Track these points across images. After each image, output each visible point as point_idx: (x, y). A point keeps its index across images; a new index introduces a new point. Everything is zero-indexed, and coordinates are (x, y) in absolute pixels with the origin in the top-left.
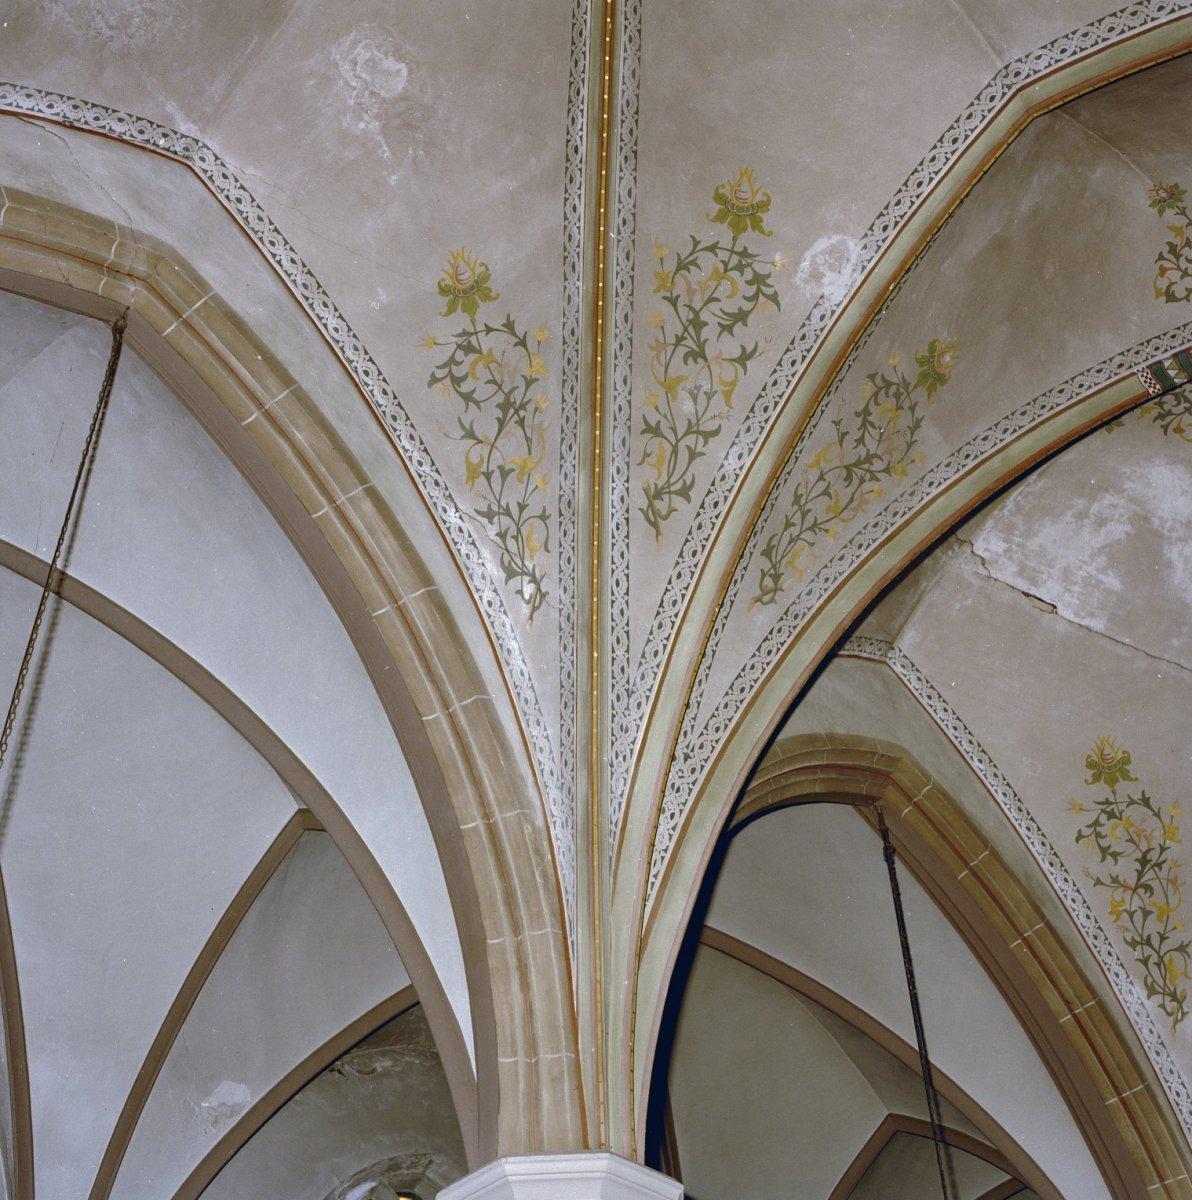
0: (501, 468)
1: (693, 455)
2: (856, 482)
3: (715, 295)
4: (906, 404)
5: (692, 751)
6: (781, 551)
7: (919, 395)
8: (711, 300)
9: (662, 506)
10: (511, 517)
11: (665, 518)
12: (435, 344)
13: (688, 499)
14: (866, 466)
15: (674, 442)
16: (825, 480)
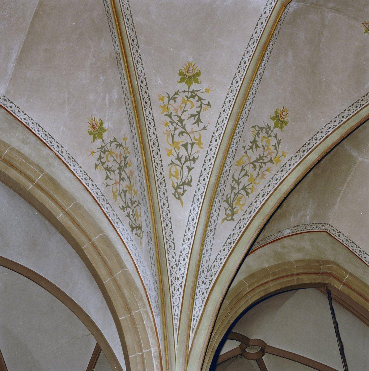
0: (123, 190)
1: (190, 169)
2: (258, 168)
3: (185, 109)
4: (273, 135)
5: (211, 268)
6: (232, 199)
7: (277, 130)
8: (184, 111)
9: (180, 191)
10: (129, 207)
11: (183, 194)
12: (94, 153)
13: (191, 186)
14: (261, 161)
15: (181, 166)
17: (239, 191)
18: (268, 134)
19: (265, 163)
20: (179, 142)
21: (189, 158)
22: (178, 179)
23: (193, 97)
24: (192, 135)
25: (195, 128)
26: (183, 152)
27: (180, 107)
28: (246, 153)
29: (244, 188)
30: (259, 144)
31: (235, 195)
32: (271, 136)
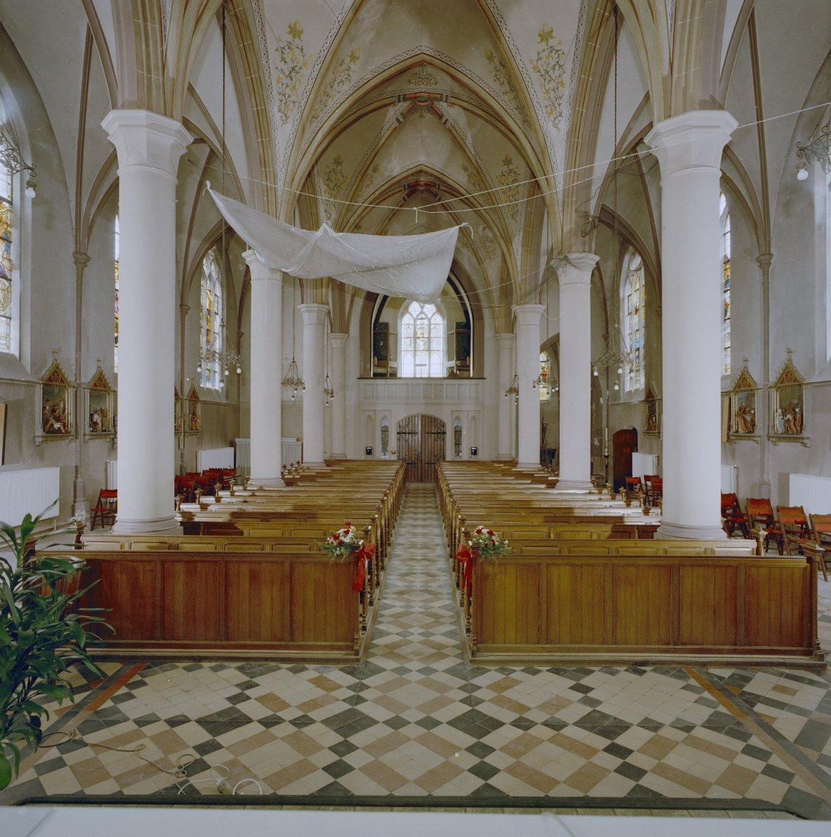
1: (559, 105)
9: (557, 122)
23: (551, 51)
24: (556, 81)
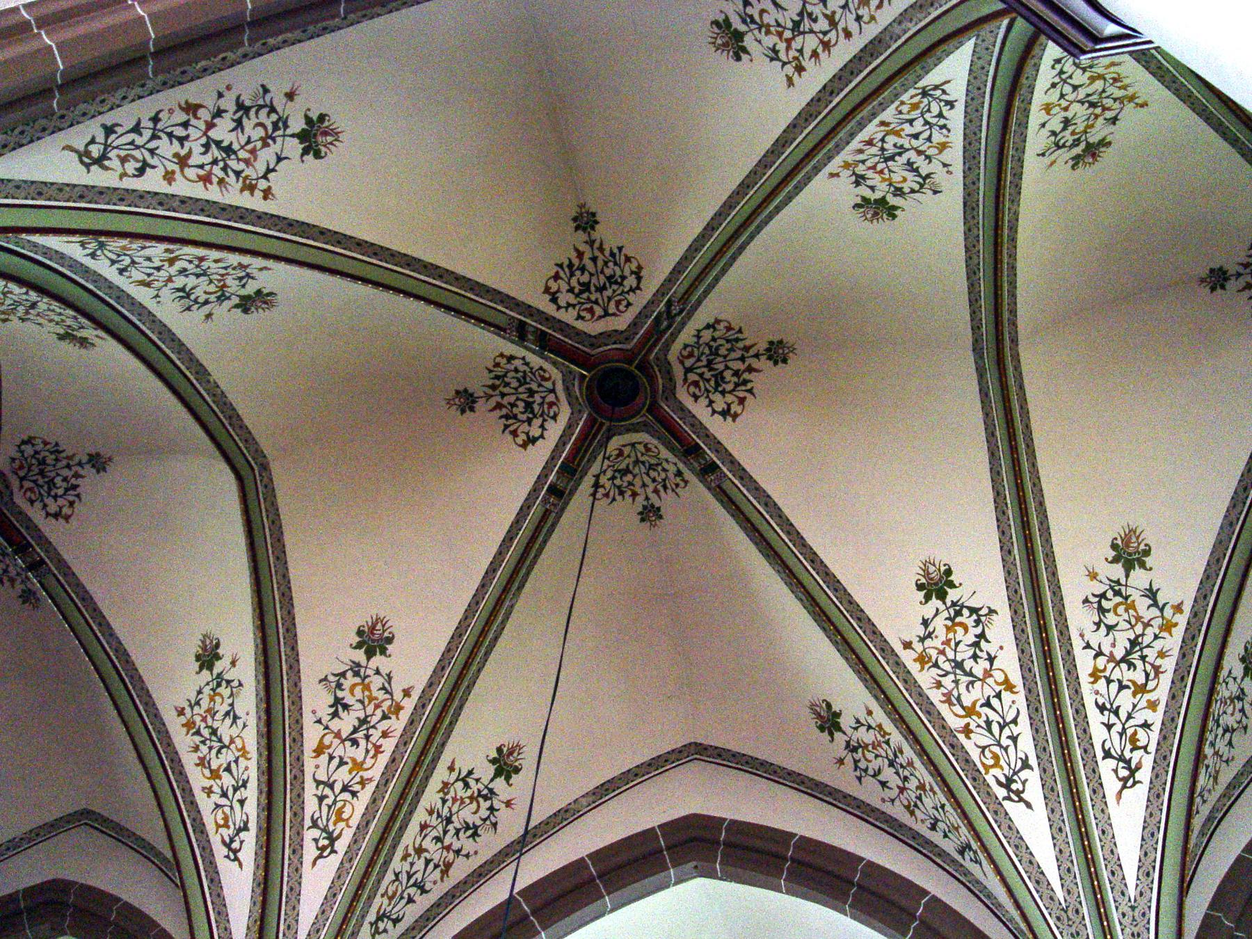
9: (235, 845)
11: (1023, 791)
16: (1113, 681)
17: (336, 797)
18: (360, 676)
19: (373, 727)
20: (974, 704)
21: (1004, 721)
22: (228, 827)
23: (219, 685)
25: (235, 731)
26: (227, 780)
27: (947, 642)
28: (327, 728)
29: (345, 788)
30: (349, 700)
31: (330, 807)
32: (369, 676)
